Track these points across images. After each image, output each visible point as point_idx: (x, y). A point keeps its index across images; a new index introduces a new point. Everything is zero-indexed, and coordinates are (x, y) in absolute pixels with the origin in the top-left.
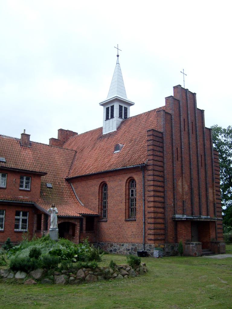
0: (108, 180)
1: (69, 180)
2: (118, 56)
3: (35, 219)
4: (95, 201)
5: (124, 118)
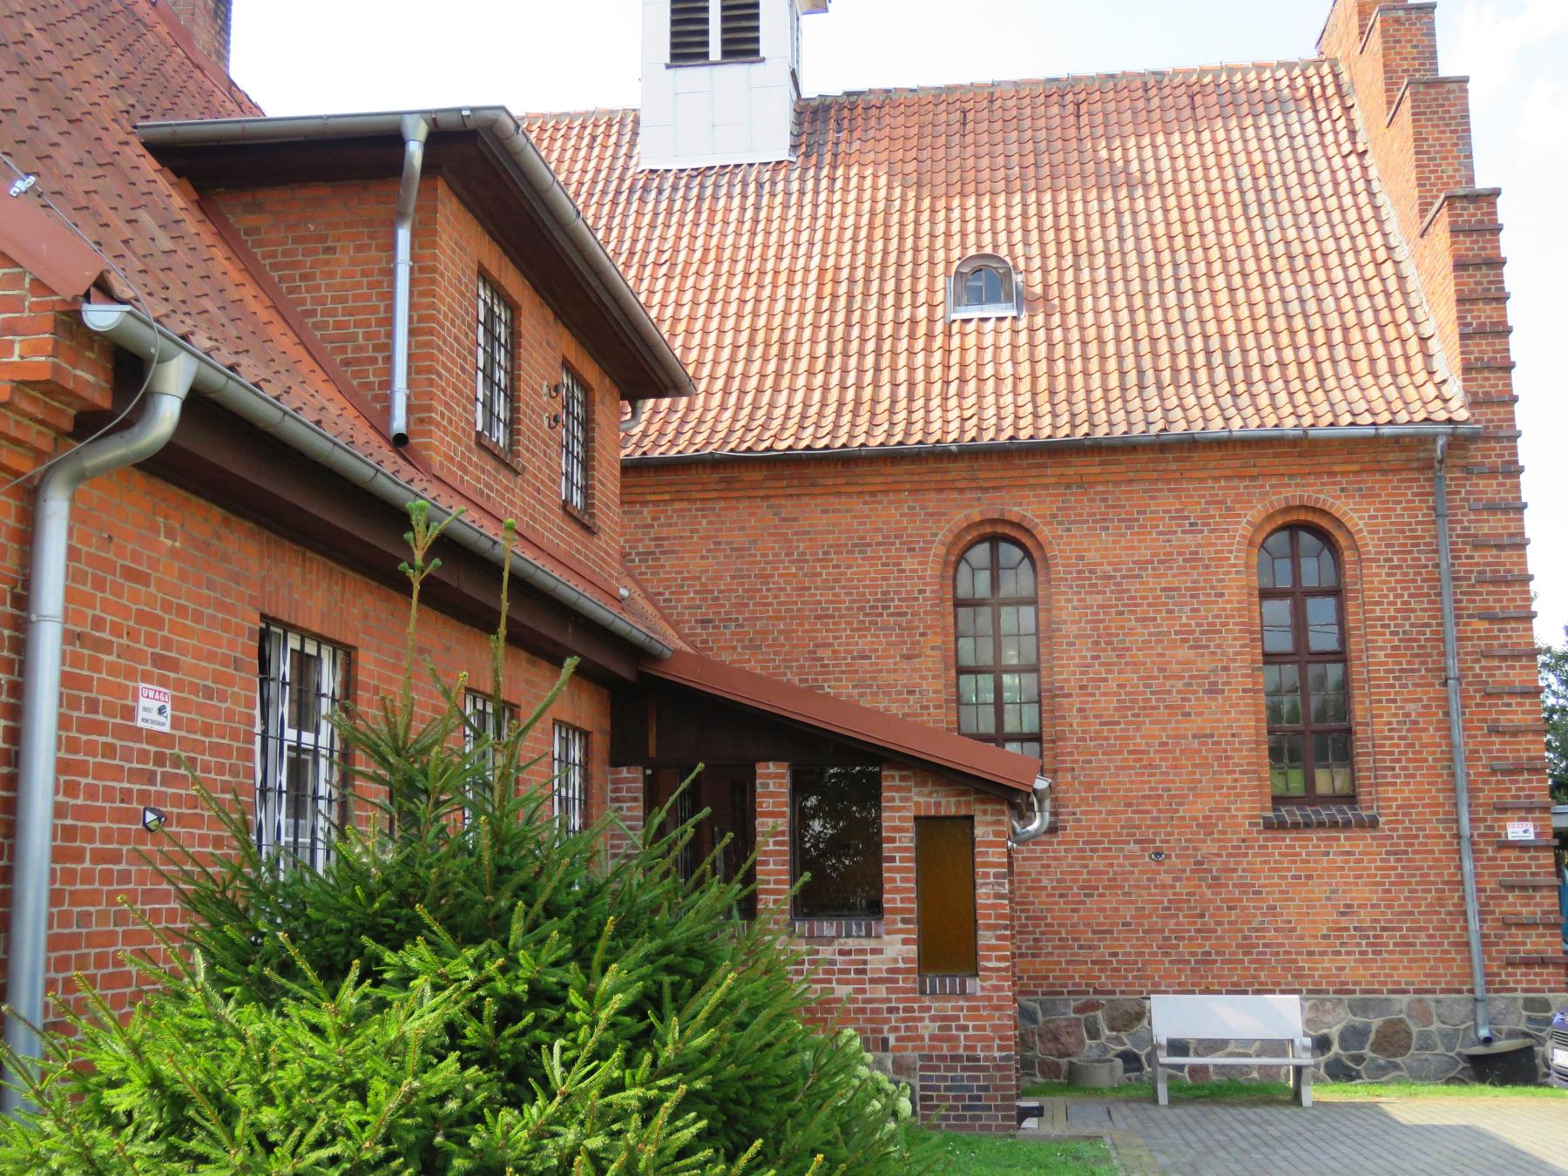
4: (905, 665)
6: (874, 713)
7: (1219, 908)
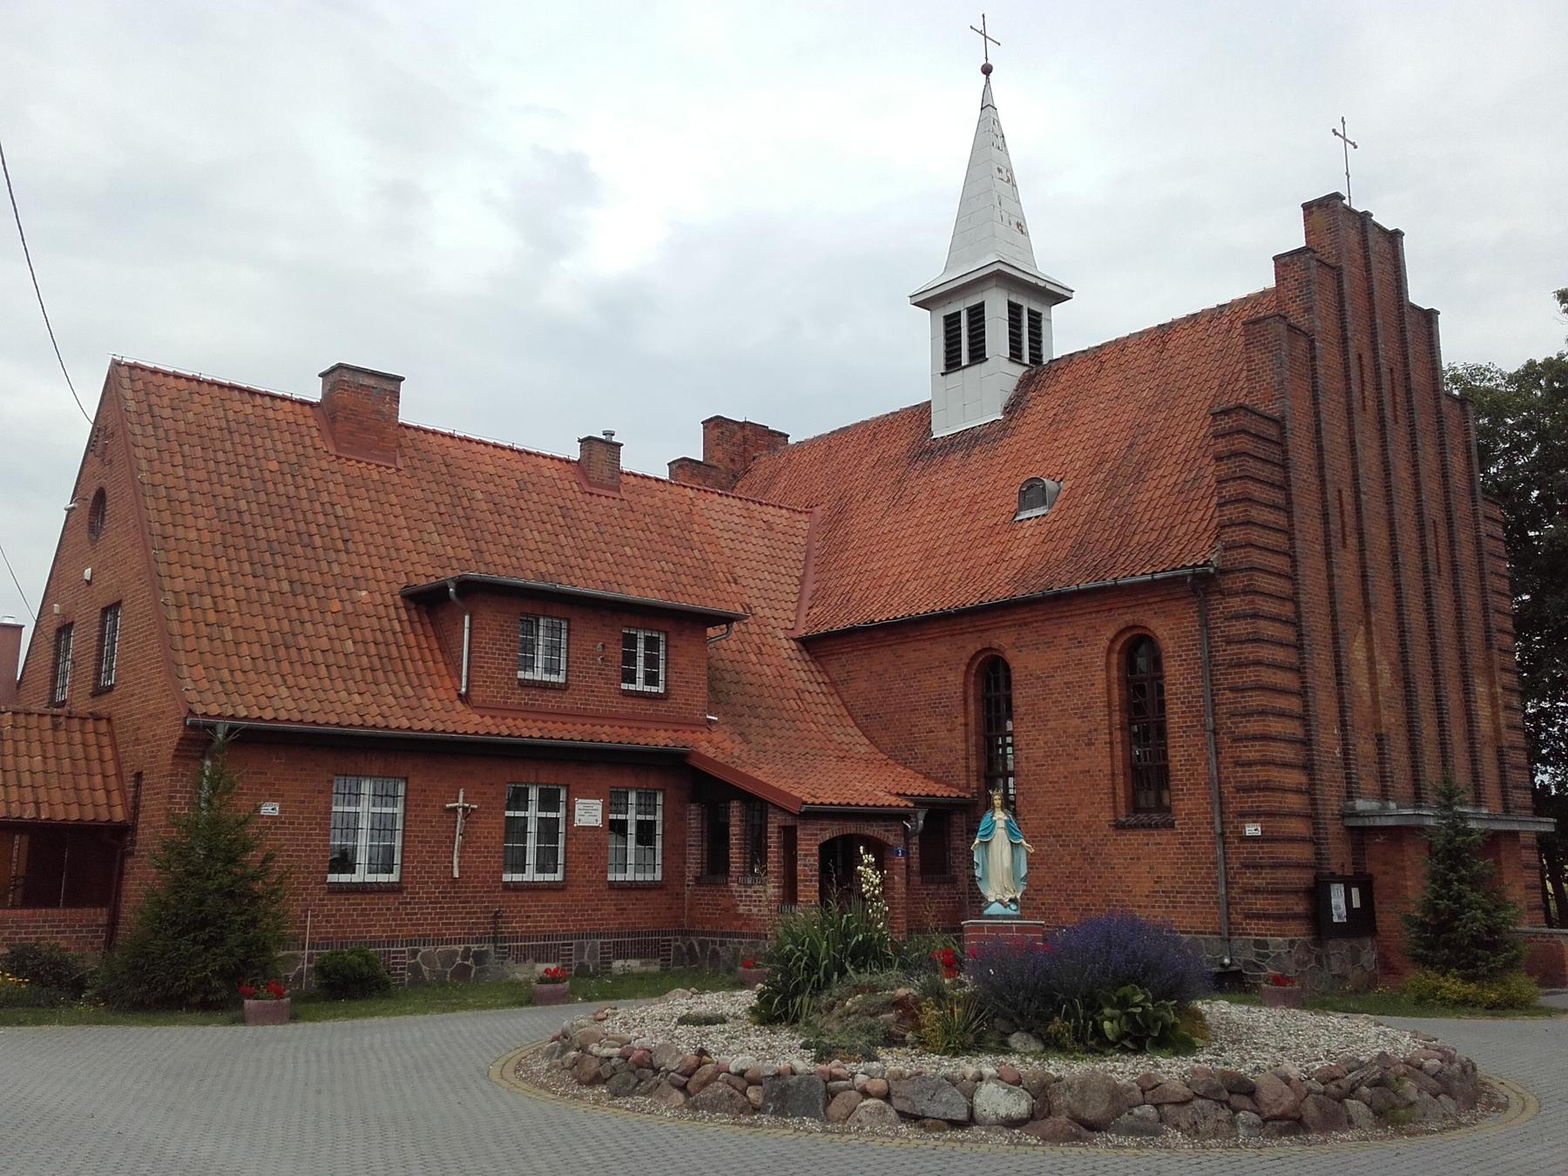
1: (815, 646)
2: (987, 70)
3: (694, 824)
5: (1031, 360)
7: (1093, 877)
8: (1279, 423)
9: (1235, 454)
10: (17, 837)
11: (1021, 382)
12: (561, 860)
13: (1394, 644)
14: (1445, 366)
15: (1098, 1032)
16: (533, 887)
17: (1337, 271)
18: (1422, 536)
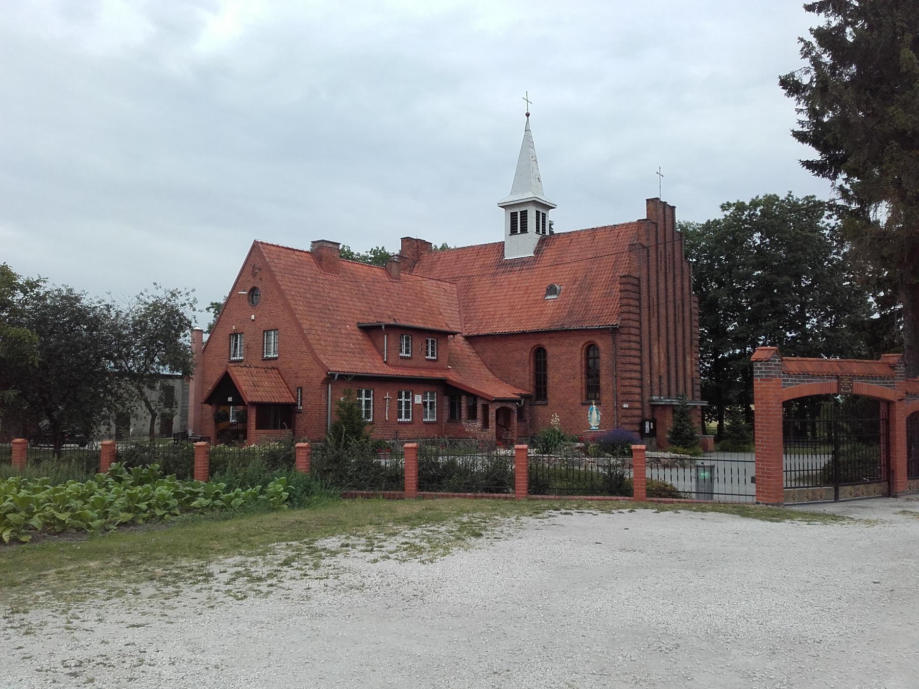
0: (547, 343)
2: (528, 115)
6: (469, 388)
8: (639, 279)
9: (626, 290)
10: (231, 407)
11: (539, 241)
12: (411, 415)
13: (665, 346)
14: (677, 221)
15: (625, 453)
16: (405, 423)
17: (656, 224)
18: (675, 310)
